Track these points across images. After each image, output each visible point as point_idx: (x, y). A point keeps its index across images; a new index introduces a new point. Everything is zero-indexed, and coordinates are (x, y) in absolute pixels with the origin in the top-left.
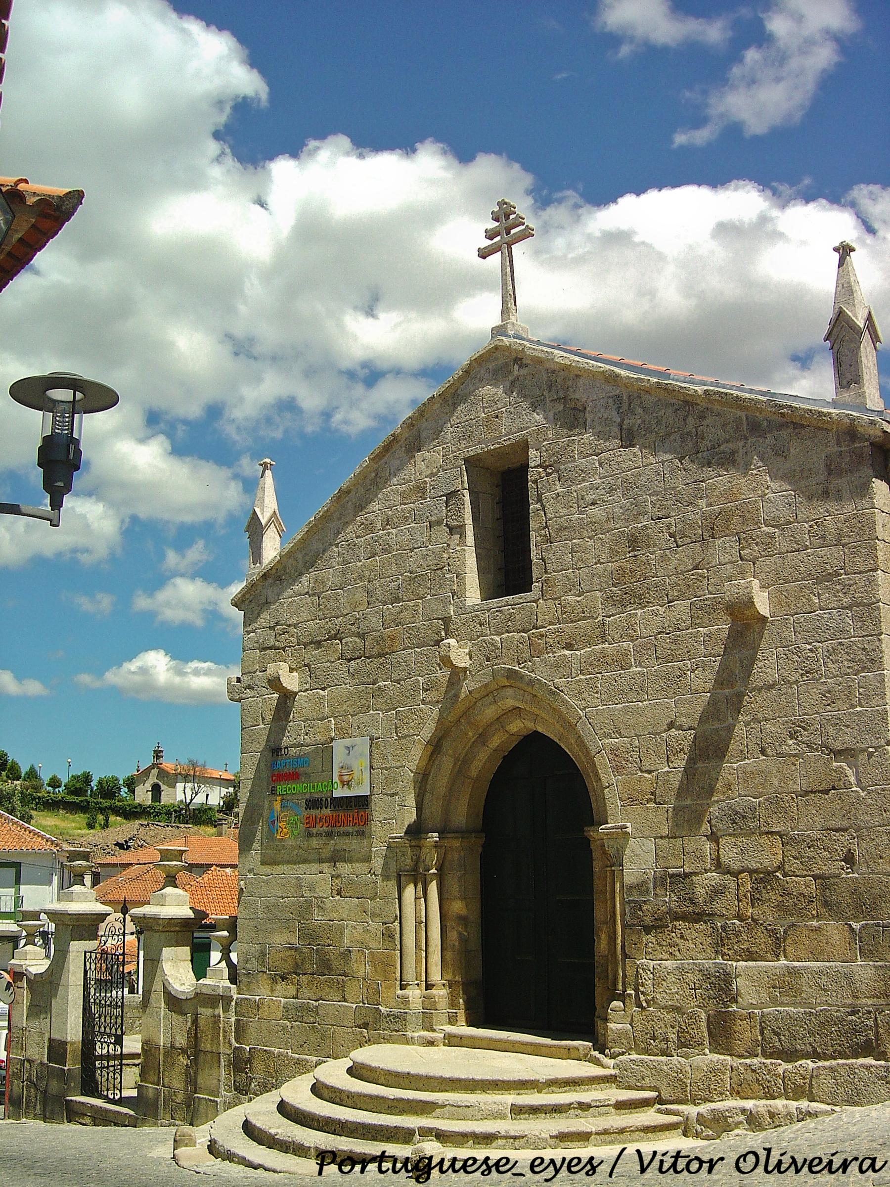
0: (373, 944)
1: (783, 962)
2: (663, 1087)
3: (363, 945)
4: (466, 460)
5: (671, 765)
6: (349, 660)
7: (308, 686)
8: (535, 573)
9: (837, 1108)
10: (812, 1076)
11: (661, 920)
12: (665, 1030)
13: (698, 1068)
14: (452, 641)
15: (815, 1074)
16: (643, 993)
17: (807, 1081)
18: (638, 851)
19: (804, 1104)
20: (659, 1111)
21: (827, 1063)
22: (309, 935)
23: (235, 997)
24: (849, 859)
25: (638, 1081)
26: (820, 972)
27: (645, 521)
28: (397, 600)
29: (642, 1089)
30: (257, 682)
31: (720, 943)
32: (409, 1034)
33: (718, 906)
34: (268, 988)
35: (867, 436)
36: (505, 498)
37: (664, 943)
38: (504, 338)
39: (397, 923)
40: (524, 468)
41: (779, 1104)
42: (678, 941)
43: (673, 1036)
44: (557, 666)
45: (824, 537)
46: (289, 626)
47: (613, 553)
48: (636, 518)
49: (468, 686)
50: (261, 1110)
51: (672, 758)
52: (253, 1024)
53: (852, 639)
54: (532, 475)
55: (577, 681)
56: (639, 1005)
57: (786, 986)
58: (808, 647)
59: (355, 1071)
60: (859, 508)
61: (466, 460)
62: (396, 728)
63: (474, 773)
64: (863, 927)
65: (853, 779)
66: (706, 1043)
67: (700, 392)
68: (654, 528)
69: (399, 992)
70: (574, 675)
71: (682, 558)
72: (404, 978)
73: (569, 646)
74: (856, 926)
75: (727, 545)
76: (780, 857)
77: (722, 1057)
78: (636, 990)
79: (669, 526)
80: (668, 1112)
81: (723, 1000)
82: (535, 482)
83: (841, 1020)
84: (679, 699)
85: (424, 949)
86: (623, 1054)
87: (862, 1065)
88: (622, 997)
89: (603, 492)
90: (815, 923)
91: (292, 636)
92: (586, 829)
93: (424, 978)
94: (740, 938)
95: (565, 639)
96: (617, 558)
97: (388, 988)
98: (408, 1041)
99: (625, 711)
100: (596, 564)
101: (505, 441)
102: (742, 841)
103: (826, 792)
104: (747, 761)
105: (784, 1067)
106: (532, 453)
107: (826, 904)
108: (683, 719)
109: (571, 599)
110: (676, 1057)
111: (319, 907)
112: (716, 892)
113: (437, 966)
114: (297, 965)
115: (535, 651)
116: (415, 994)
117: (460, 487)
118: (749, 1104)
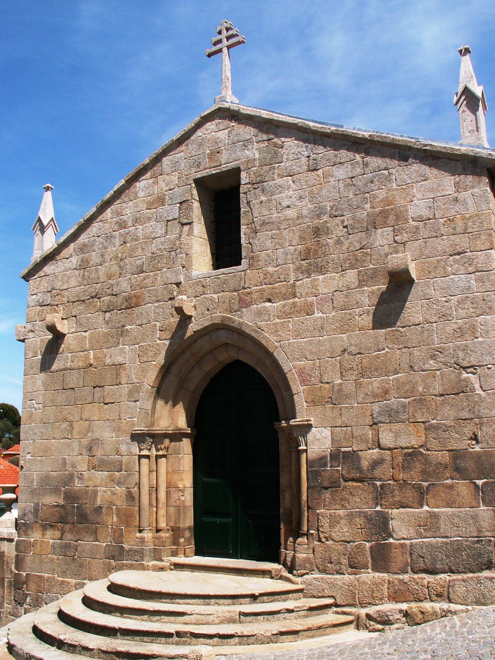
0: (119, 503)
1: (426, 508)
2: (338, 596)
3: (112, 503)
4: (196, 181)
5: (344, 379)
6: (106, 312)
7: (73, 330)
8: (244, 254)
9: (470, 608)
10: (449, 586)
11: (335, 482)
12: (338, 557)
13: (364, 583)
14: (184, 297)
15: (451, 584)
16: (322, 532)
17: (446, 589)
18: (319, 436)
19: (445, 606)
20: (337, 613)
21: (460, 577)
22: (71, 497)
23: (16, 539)
24: (475, 438)
25: (319, 592)
26: (454, 515)
27: (325, 218)
28: (142, 272)
29: (323, 597)
30: (37, 328)
31: (380, 495)
32: (163, 558)
33: (377, 473)
34: (40, 532)
35: (484, 165)
36: (222, 203)
37: (337, 498)
38: (225, 103)
39: (136, 488)
40: (238, 185)
41: (427, 606)
42: (348, 497)
43: (345, 561)
44: (259, 313)
45: (454, 229)
46: (61, 290)
47: (302, 238)
48: (319, 216)
49: (193, 328)
50: (46, 618)
51: (344, 374)
52: (29, 558)
53: (475, 294)
54: (242, 189)
55: (274, 324)
56: (320, 540)
57: (430, 524)
58: (444, 299)
59: (114, 588)
60: (479, 210)
61: (196, 181)
62: (139, 356)
63: (192, 387)
64: (484, 484)
65: (477, 386)
66: (370, 565)
67: (367, 136)
68: (332, 223)
69: (138, 535)
70: (272, 320)
71: (355, 241)
72: (142, 525)
73: (269, 301)
74: (480, 482)
75: (385, 233)
76: (423, 439)
77: (381, 575)
78: (318, 530)
79: (343, 222)
80: (344, 613)
81: (382, 536)
82: (245, 193)
83: (470, 548)
84: (350, 335)
85: (155, 505)
86: (307, 573)
87: (486, 578)
88: (307, 535)
89: (294, 200)
90: (449, 481)
91: (63, 297)
92: (275, 423)
93: (154, 525)
94: (394, 494)
95: (266, 295)
96: (303, 243)
97: (129, 532)
98: (144, 568)
99: (310, 343)
100: (290, 246)
101: (224, 168)
102: (397, 427)
103: (457, 394)
104: (400, 375)
105: (428, 578)
106: (243, 175)
107: (457, 469)
108: (353, 348)
109: (270, 269)
110: (347, 575)
111: (79, 477)
112: (376, 464)
113: (164, 516)
114: (62, 517)
115: (244, 303)
116: (148, 535)
117: (190, 198)
118: (404, 606)
